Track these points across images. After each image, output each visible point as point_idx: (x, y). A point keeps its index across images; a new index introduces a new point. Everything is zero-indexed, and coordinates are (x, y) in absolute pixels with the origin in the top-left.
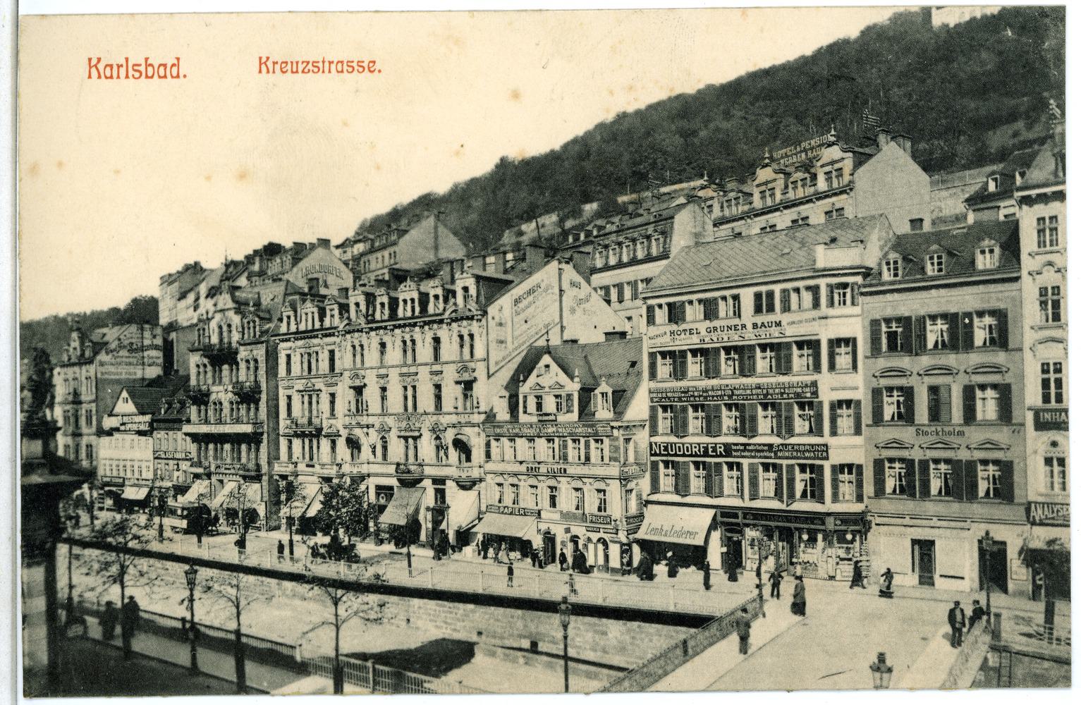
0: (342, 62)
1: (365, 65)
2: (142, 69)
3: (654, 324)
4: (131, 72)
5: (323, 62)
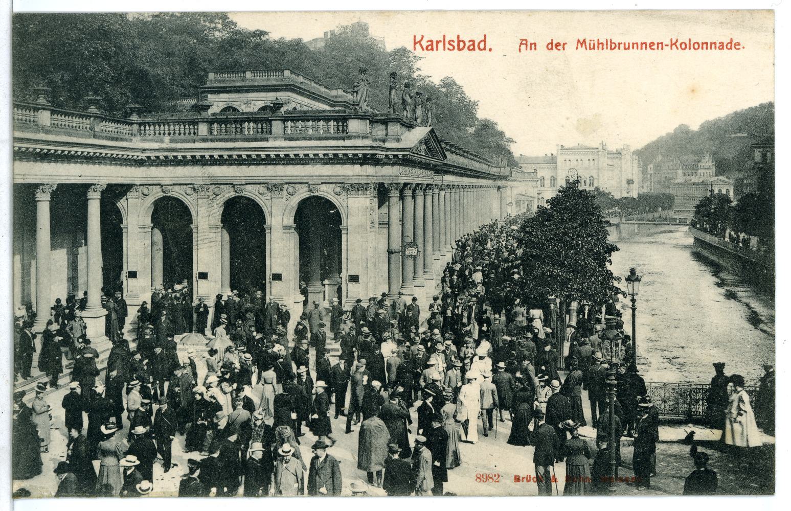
2: (455, 44)
4: (447, 46)
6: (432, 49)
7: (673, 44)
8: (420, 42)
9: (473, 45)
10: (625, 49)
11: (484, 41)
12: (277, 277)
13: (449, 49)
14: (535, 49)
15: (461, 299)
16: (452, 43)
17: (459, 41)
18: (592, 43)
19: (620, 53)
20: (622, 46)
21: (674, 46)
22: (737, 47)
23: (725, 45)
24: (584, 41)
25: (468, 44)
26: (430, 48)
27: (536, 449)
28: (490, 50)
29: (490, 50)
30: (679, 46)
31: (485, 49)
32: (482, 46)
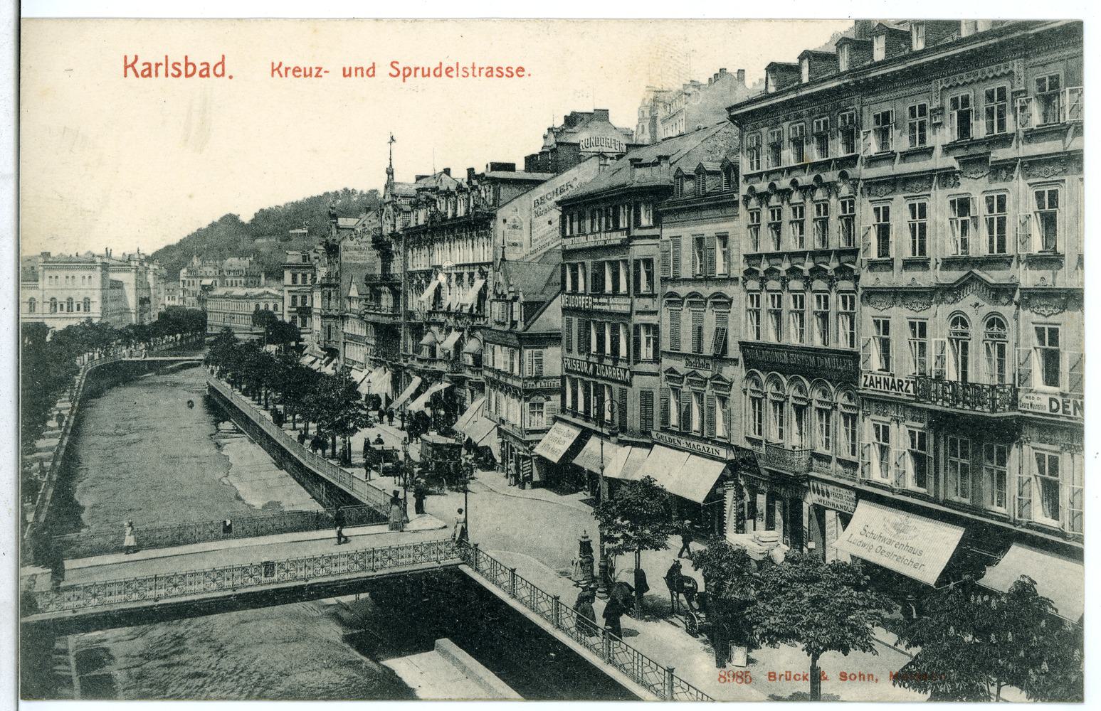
0: (187, 76)
1: (514, 71)
2: (182, 68)
3: (423, 512)
4: (171, 70)
5: (474, 68)
6: (150, 75)
8: (132, 65)
9: (208, 69)
10: (423, 76)
11: (222, 63)
13: (173, 75)
14: (344, 69)
15: (171, 257)
16: (177, 66)
17: (187, 64)
19: (456, 82)
21: (276, 72)
22: (520, 73)
25: (199, 68)
26: (205, 73)
27: (927, 587)
29: (231, 77)
31: (223, 74)
32: (219, 70)
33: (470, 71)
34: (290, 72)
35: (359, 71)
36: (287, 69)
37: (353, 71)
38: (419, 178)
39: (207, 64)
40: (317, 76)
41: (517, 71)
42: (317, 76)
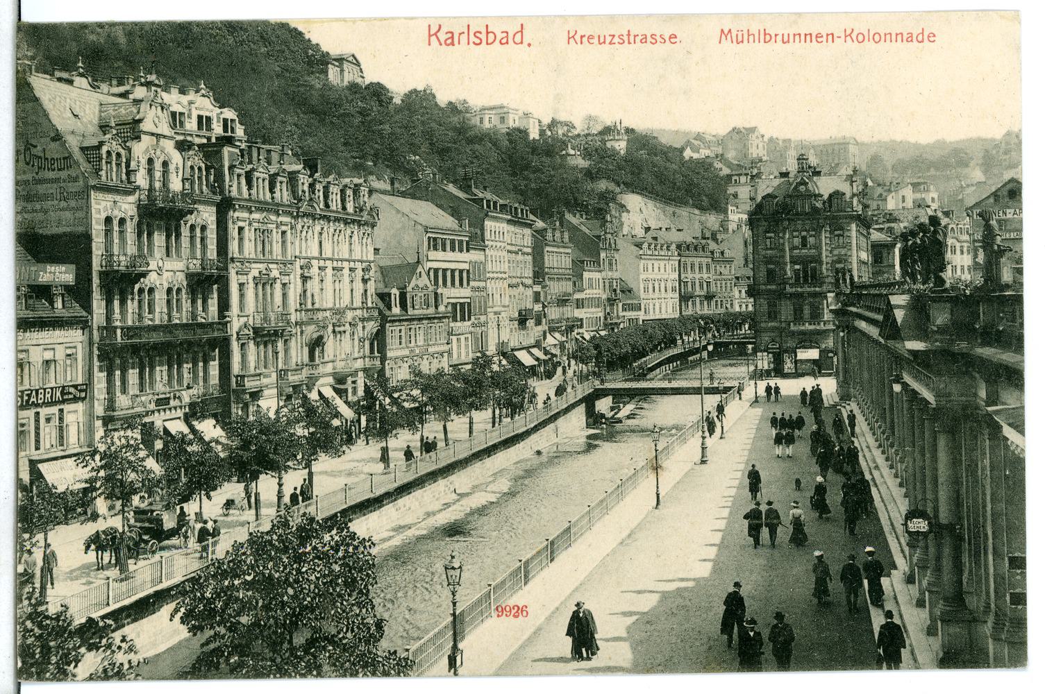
2: (483, 36)
4: (472, 38)
5: (629, 35)
7: (848, 35)
8: (435, 34)
12: (334, 369)
13: (474, 43)
16: (478, 35)
18: (740, 34)
20: (779, 38)
21: (848, 38)
22: (932, 39)
23: (511, 36)
24: (730, 31)
28: (529, 45)
30: (855, 38)
31: (522, 43)
32: (518, 38)
33: (626, 38)
34: (585, 39)
35: (808, 37)
36: (582, 37)
37: (791, 40)
38: (70, 82)
39: (452, 33)
40: (610, 43)
41: (670, 38)
42: (610, 43)
